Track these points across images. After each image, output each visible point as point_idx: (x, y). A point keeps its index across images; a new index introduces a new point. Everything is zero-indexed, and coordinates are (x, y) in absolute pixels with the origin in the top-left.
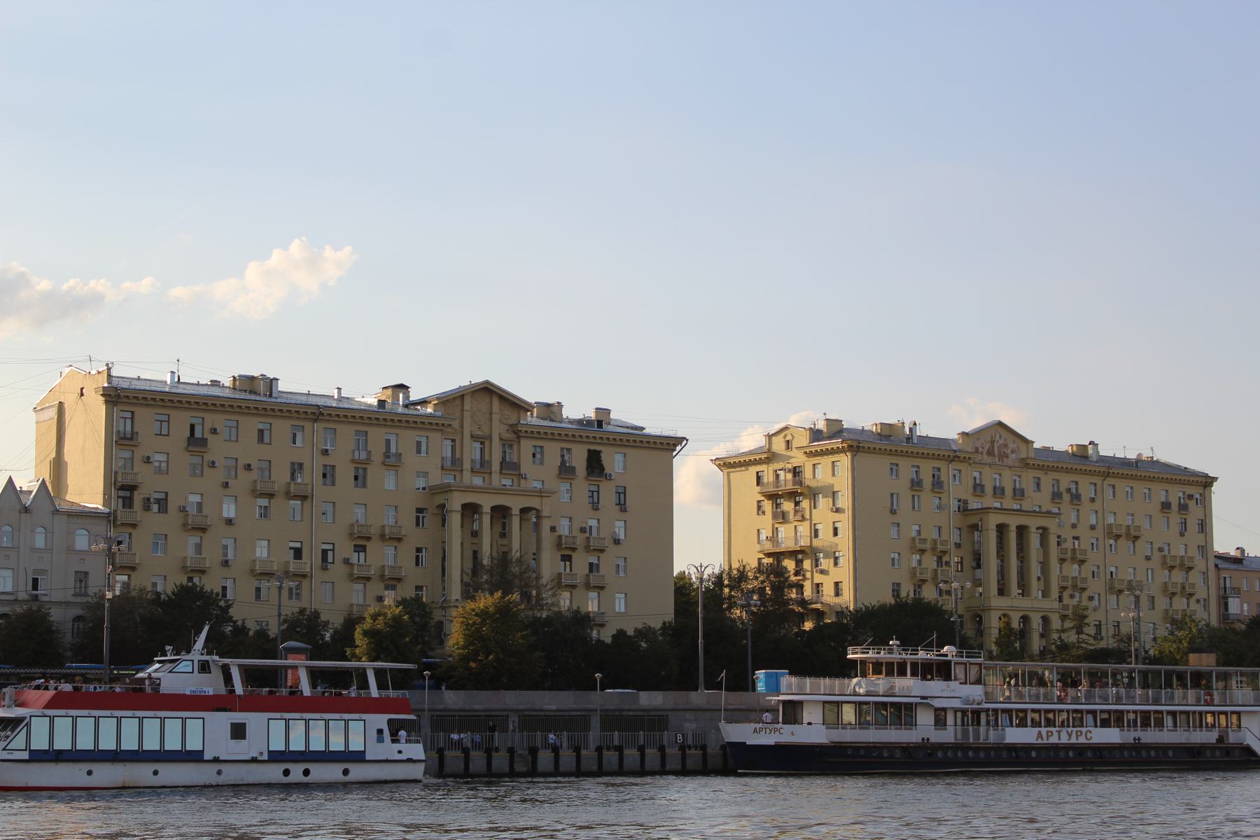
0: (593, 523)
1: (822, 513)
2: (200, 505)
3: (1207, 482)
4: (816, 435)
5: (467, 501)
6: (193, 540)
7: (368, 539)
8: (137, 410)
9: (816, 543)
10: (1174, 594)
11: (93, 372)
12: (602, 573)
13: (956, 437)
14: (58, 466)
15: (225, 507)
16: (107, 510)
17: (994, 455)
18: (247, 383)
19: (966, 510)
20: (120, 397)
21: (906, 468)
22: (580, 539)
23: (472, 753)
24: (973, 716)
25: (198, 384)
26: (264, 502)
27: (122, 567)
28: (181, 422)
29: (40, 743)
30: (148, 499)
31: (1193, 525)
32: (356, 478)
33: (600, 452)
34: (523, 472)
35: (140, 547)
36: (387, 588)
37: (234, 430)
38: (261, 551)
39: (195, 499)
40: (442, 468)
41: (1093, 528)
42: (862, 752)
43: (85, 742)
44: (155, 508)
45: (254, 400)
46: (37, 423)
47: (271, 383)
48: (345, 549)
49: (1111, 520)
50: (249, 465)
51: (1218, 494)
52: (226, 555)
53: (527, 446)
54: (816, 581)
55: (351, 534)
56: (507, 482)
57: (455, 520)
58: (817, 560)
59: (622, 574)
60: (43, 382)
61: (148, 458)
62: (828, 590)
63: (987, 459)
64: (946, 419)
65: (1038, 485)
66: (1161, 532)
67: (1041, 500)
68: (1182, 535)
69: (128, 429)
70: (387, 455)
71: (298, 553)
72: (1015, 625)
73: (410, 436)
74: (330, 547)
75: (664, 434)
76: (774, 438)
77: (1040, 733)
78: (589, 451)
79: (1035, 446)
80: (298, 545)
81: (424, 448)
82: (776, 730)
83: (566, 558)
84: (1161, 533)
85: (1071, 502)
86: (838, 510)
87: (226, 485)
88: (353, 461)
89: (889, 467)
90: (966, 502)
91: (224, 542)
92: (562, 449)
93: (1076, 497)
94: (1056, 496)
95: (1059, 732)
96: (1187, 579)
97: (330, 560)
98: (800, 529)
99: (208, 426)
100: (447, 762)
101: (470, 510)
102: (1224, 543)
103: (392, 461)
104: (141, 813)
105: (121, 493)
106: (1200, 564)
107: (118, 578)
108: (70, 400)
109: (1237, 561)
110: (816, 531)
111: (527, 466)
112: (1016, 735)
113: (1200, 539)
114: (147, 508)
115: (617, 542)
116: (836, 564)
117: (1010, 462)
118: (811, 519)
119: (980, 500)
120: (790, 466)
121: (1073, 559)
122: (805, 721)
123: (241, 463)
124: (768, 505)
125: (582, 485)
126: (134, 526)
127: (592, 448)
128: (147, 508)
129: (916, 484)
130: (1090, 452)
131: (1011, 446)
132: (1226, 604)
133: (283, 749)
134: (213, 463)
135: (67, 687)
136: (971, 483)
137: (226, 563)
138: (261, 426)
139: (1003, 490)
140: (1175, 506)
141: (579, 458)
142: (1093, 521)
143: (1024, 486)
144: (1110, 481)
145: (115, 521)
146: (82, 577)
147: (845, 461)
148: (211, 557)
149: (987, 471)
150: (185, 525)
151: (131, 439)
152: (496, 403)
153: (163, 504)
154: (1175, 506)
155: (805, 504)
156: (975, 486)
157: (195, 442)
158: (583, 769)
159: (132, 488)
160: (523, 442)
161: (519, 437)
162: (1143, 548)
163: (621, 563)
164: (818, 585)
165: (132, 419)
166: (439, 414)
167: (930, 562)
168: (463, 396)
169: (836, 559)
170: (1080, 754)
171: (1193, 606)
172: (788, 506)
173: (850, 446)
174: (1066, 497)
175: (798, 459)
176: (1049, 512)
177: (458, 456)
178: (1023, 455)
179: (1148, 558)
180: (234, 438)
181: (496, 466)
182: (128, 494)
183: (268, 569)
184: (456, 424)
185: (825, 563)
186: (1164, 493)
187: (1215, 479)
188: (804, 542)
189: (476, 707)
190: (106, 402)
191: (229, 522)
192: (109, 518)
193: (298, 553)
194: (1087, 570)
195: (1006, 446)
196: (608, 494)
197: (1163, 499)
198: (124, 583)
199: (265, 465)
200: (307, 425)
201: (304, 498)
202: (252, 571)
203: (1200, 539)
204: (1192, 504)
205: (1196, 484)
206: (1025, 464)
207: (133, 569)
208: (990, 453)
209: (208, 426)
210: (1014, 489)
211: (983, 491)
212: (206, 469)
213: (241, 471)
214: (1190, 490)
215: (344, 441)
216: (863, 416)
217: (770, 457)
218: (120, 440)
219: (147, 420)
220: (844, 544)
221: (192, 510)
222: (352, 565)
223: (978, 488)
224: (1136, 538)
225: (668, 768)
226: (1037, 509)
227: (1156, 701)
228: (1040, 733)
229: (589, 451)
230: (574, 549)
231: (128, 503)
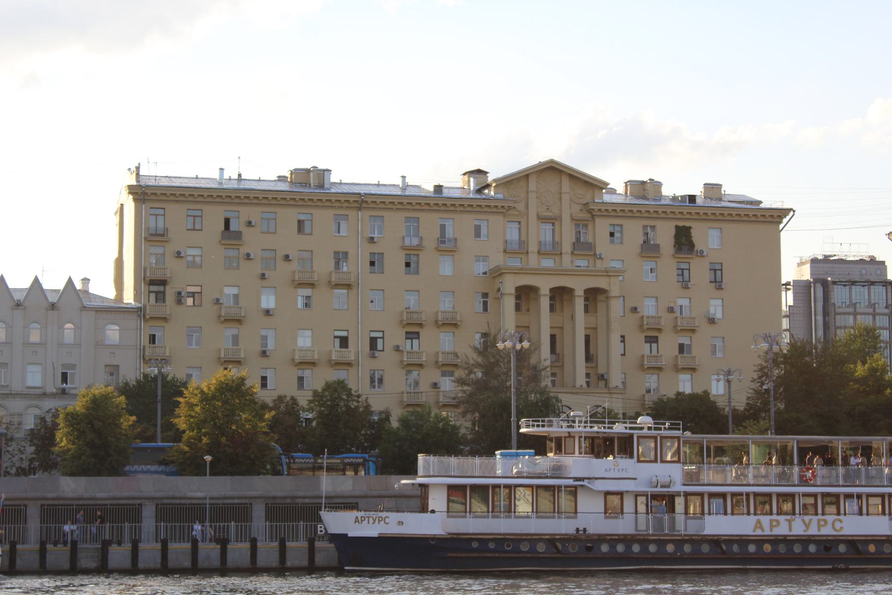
0: (685, 302)
2: (236, 297)
5: (592, 286)
6: (230, 331)
7: (420, 325)
12: (693, 354)
22: (666, 320)
23: (201, 545)
24: (664, 500)
26: (307, 292)
28: (214, 216)
32: (408, 265)
33: (690, 227)
34: (598, 253)
35: (171, 340)
36: (444, 374)
38: (304, 341)
39: (230, 291)
40: (505, 251)
42: (492, 546)
44: (190, 301)
45: (309, 192)
47: (323, 174)
48: (395, 336)
53: (602, 227)
55: (641, 326)
56: (582, 263)
57: (509, 303)
59: (719, 355)
61: (179, 253)
70: (442, 240)
71: (344, 342)
73: (468, 221)
74: (380, 335)
75: (774, 206)
77: (759, 522)
78: (677, 227)
80: (344, 334)
81: (484, 231)
82: (381, 519)
83: (652, 340)
87: (263, 277)
88: (404, 248)
91: (263, 332)
92: (645, 227)
95: (789, 521)
97: (380, 347)
100: (171, 557)
101: (525, 294)
103: (446, 246)
111: (603, 245)
112: (720, 525)
115: (712, 321)
122: (430, 509)
123: (280, 254)
125: (668, 263)
127: (681, 224)
134: (248, 255)
137: (264, 354)
141: (665, 235)
146: (113, 370)
148: (249, 347)
151: (163, 235)
152: (566, 182)
158: (171, 564)
160: (598, 220)
161: (593, 217)
163: (719, 343)
166: (500, 196)
168: (527, 176)
170: (827, 549)
177: (557, 239)
181: (567, 247)
183: (309, 358)
184: (521, 207)
189: (99, 495)
190: (135, 200)
191: (267, 312)
192: (138, 312)
193: (344, 342)
196: (700, 271)
200: (352, 214)
201: (348, 286)
209: (244, 219)
213: (280, 263)
215: (393, 231)
218: (150, 237)
219: (176, 217)
222: (402, 352)
225: (289, 563)
228: (759, 522)
229: (677, 227)
230: (659, 330)
231: (160, 297)
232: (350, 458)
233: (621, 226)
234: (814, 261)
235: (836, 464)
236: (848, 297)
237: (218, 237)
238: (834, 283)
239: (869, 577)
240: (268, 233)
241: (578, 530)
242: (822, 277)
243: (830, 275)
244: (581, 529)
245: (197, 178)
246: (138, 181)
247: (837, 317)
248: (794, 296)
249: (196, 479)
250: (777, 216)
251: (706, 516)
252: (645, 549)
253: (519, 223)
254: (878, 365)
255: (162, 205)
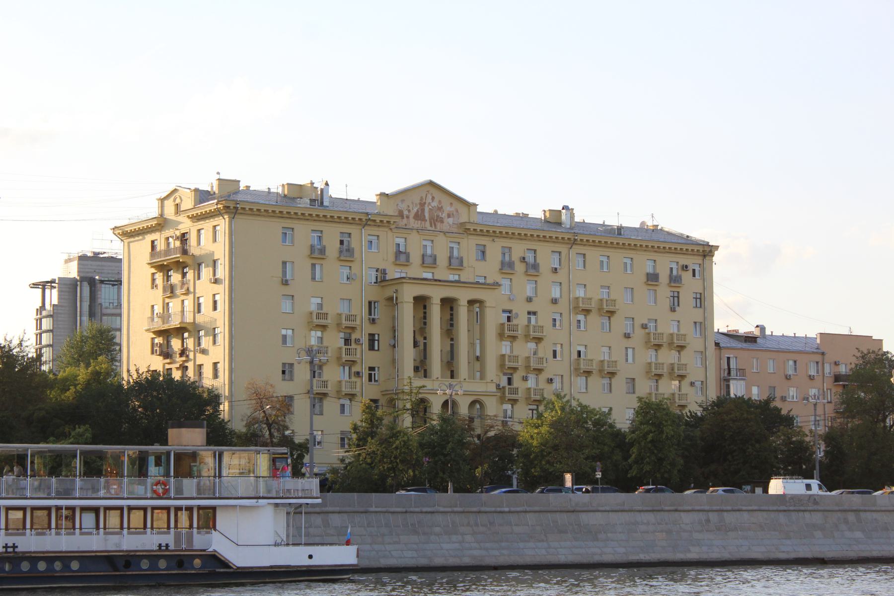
1: (204, 288)
3: (706, 251)
4: (202, 196)
9: (200, 319)
10: (660, 376)
13: (374, 199)
17: (424, 220)
18: (296, 192)
19: (384, 280)
21: (304, 233)
31: (687, 298)
41: (555, 301)
49: (580, 293)
51: (720, 265)
54: (198, 363)
58: (199, 338)
62: (207, 372)
63: (413, 223)
64: (359, 181)
65: (483, 253)
66: (649, 307)
67: (489, 269)
68: (673, 310)
76: (166, 202)
79: (479, 209)
84: (649, 307)
85: (526, 273)
86: (216, 281)
89: (281, 231)
90: (384, 272)
93: (533, 268)
94: (507, 267)
96: (679, 359)
98: (186, 303)
102: (723, 321)
106: (694, 342)
109: (750, 339)
110: (199, 305)
113: (697, 315)
116: (214, 343)
117: (445, 227)
118: (194, 293)
119: (405, 269)
120: (178, 233)
121: (527, 337)
124: (159, 277)
129: (317, 253)
130: (563, 217)
131: (448, 209)
132: (728, 387)
136: (392, 250)
139: (323, 251)
140: (664, 278)
142: (556, 293)
143: (464, 254)
144: (577, 249)
147: (223, 223)
149: (414, 237)
154: (664, 278)
155: (190, 275)
156: (398, 253)
162: (619, 324)
164: (200, 366)
167: (334, 340)
169: (215, 336)
171: (686, 388)
172: (175, 278)
173: (227, 207)
174: (520, 267)
175: (186, 225)
176: (478, 283)
178: (464, 219)
179: (627, 336)
185: (206, 342)
186: (651, 263)
187: (717, 247)
188: (189, 319)
194: (545, 350)
195: (440, 209)
197: (651, 271)
203: (697, 315)
204: (686, 276)
205: (693, 253)
206: (466, 230)
208: (419, 216)
210: (450, 258)
211: (408, 260)
214: (684, 260)
216: (264, 177)
217: (161, 224)
220: (220, 319)
223: (401, 256)
224: (611, 313)
226: (482, 280)
227: (66, 494)
234: (82, 258)
235: (122, 476)
236: (116, 297)
238: (102, 282)
239: (217, 589)
241: (160, 545)
242: (90, 275)
243: (98, 274)
244: (164, 544)
247: (104, 318)
248: (59, 295)
249: (438, 496)
251: (125, 531)
252: (66, 567)
253: (560, 253)
254: (101, 368)
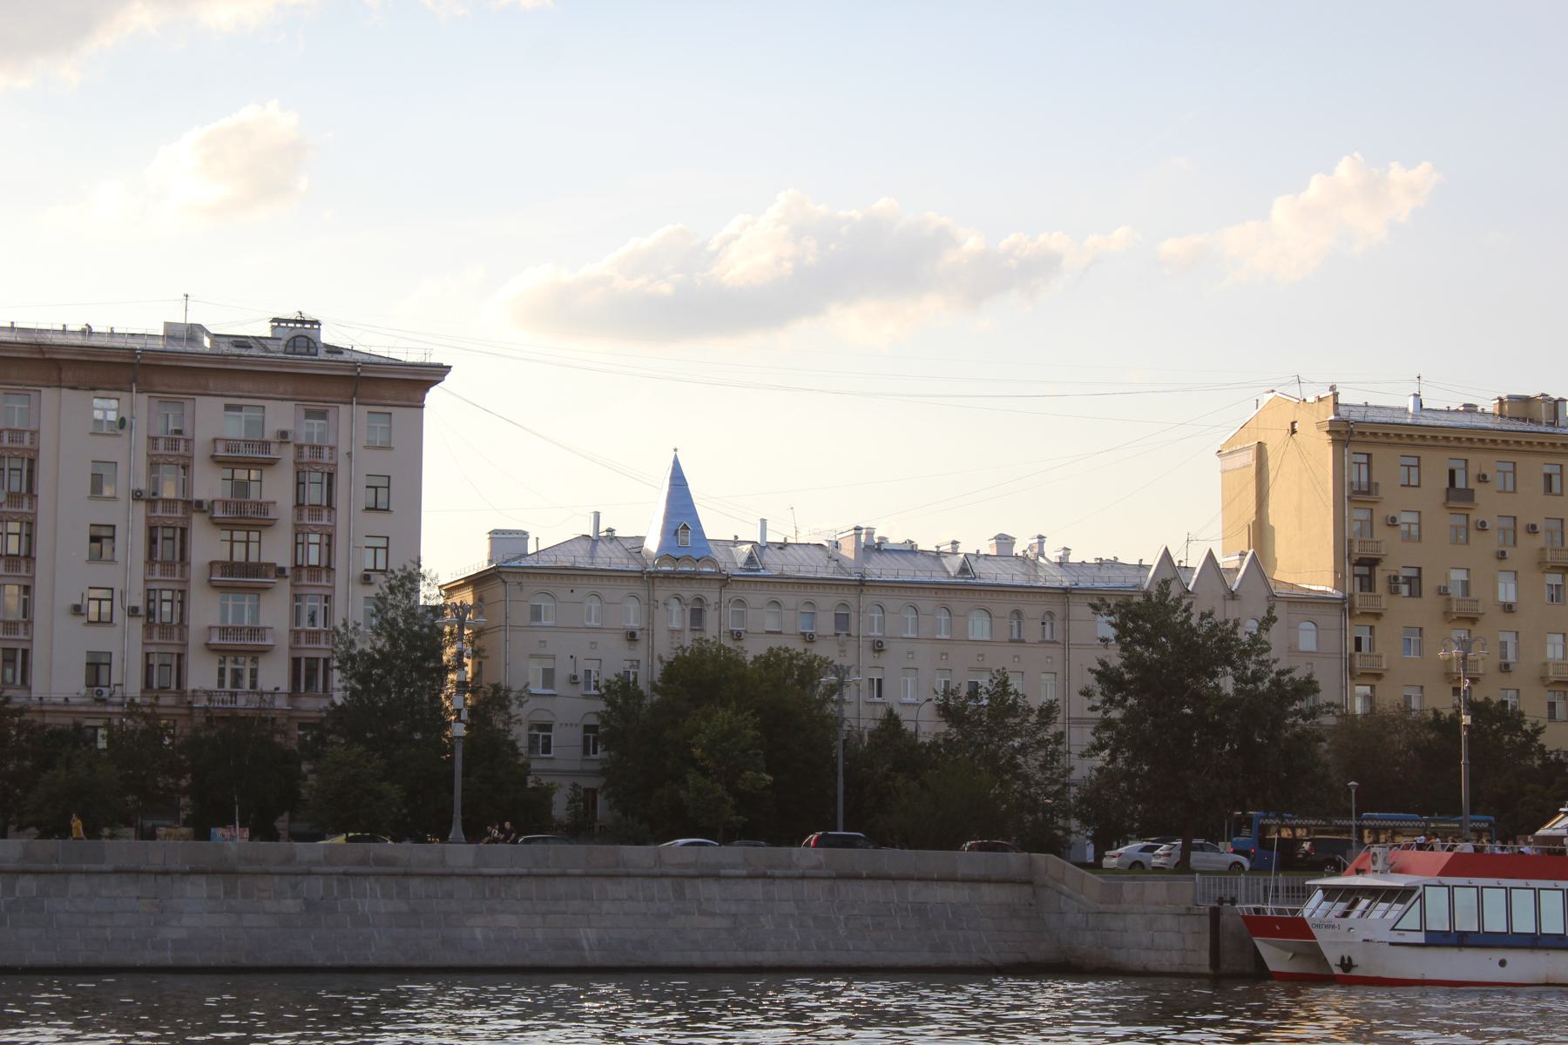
8: (1377, 452)
11: (1311, 399)
14: (1261, 532)
15: (1501, 587)
16: (1340, 595)
18: (1520, 407)
20: (1354, 434)
25: (1448, 411)
27: (1363, 674)
28: (1437, 465)
29: (1438, 923)
30: (1396, 578)
35: (1388, 647)
37: (1510, 476)
43: (1495, 923)
44: (1405, 589)
46: (1224, 472)
50: (1534, 527)
52: (1504, 656)
60: (1232, 413)
61: (1394, 519)
69: (1364, 479)
72: (1099, 668)
87: (1502, 556)
91: (1503, 637)
99: (1474, 471)
104: (901, 1033)
105: (1358, 570)
107: (1358, 689)
108: (1275, 441)
114: (1394, 591)
126: (1377, 616)
128: (1394, 591)
133: (1533, 930)
134: (1483, 524)
135: (1467, 848)
137: (1505, 668)
138: (1547, 469)
145: (1352, 608)
148: (1483, 658)
150: (1447, 613)
151: (1368, 493)
153: (1415, 584)
157: (1457, 495)
159: (1372, 563)
165: (1369, 464)
180: (1510, 487)
182: (1365, 570)
191: (1508, 608)
192: (1344, 606)
198: (1366, 697)
199: (1556, 525)
202: (1543, 678)
207: (1378, 676)
209: (1474, 471)
212: (1473, 534)
213: (1473, 534)
218: (1355, 495)
219: (1389, 465)
221: (1456, 592)
231: (1367, 583)
232: (1372, 819)
233: (1369, 455)
237: (1442, 498)
240: (1504, 491)
245: (64, 331)
246: (1336, 414)
250: (409, 384)
255: (1560, 461)
